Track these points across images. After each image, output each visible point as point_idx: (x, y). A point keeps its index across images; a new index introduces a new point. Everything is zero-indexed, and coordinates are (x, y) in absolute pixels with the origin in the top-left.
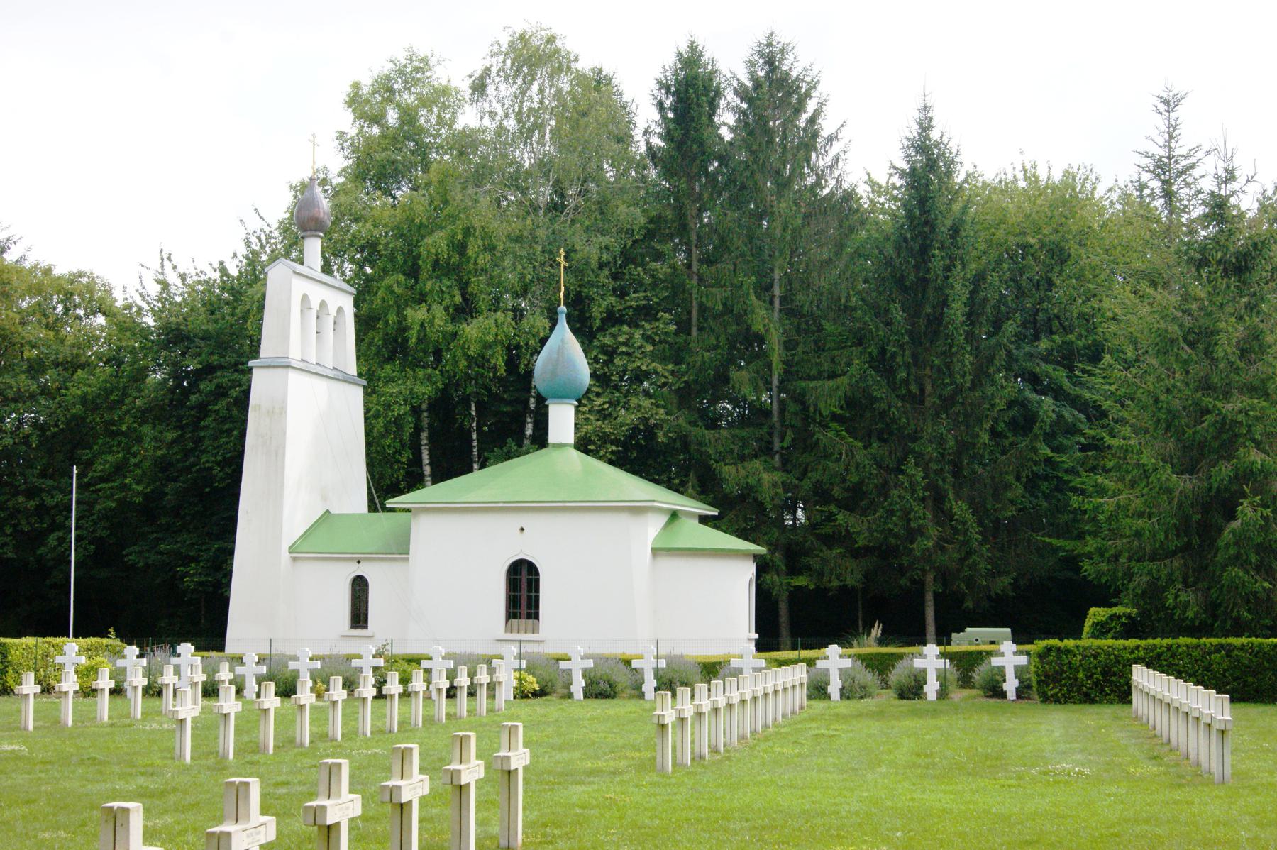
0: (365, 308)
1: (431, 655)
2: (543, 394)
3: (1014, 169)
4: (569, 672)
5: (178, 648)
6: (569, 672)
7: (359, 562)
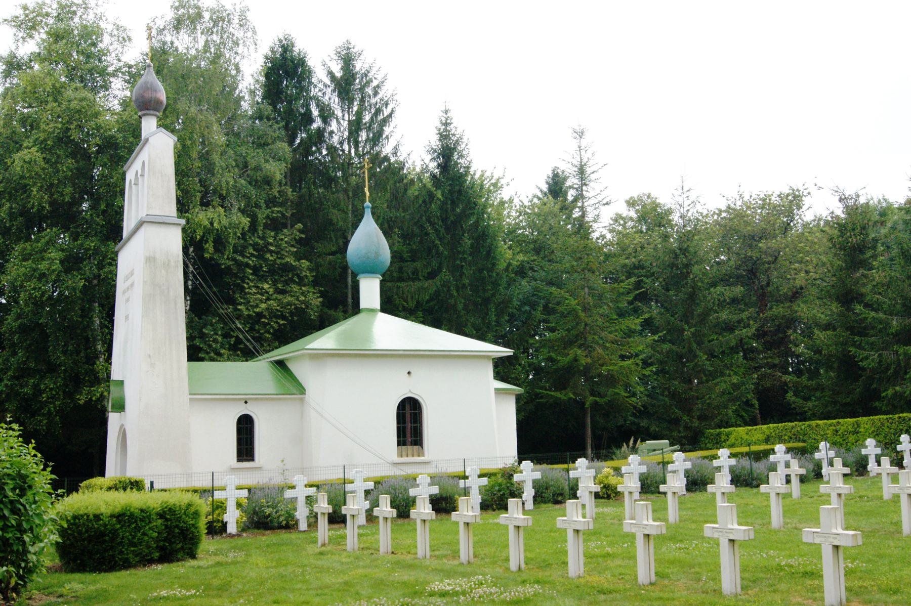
0: (380, 222)
1: (294, 484)
2: (356, 272)
3: (751, 196)
4: (294, 500)
5: (540, 477)
6: (294, 500)
7: (246, 402)
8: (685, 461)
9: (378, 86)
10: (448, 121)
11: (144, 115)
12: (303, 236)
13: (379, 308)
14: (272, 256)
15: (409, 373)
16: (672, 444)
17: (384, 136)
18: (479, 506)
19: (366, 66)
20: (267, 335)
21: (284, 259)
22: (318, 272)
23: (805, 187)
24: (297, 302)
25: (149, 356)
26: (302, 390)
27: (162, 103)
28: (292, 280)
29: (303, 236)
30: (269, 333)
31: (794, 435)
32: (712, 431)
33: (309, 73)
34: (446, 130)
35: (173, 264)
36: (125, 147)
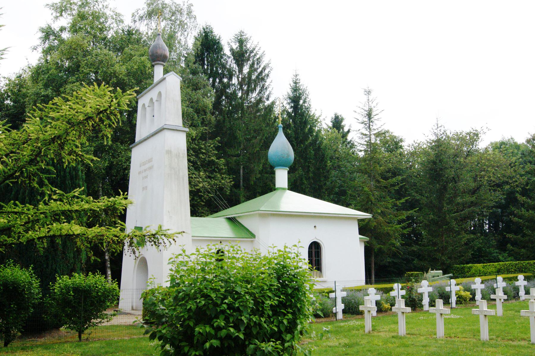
6: (421, 294)
8: (428, 286)
9: (259, 58)
10: (297, 81)
11: (156, 64)
12: (220, 145)
13: (287, 187)
14: (203, 156)
15: (315, 227)
16: (444, 273)
17: (265, 88)
18: (341, 311)
19: (253, 46)
20: (202, 203)
21: (210, 158)
22: (228, 166)
23: (482, 129)
24: (220, 184)
25: (169, 212)
26: (253, 236)
27: (167, 57)
28: (214, 171)
29: (220, 145)
30: (203, 202)
31: (518, 268)
32: (458, 266)
33: (220, 49)
34: (296, 87)
35: (181, 155)
36: (129, 85)
